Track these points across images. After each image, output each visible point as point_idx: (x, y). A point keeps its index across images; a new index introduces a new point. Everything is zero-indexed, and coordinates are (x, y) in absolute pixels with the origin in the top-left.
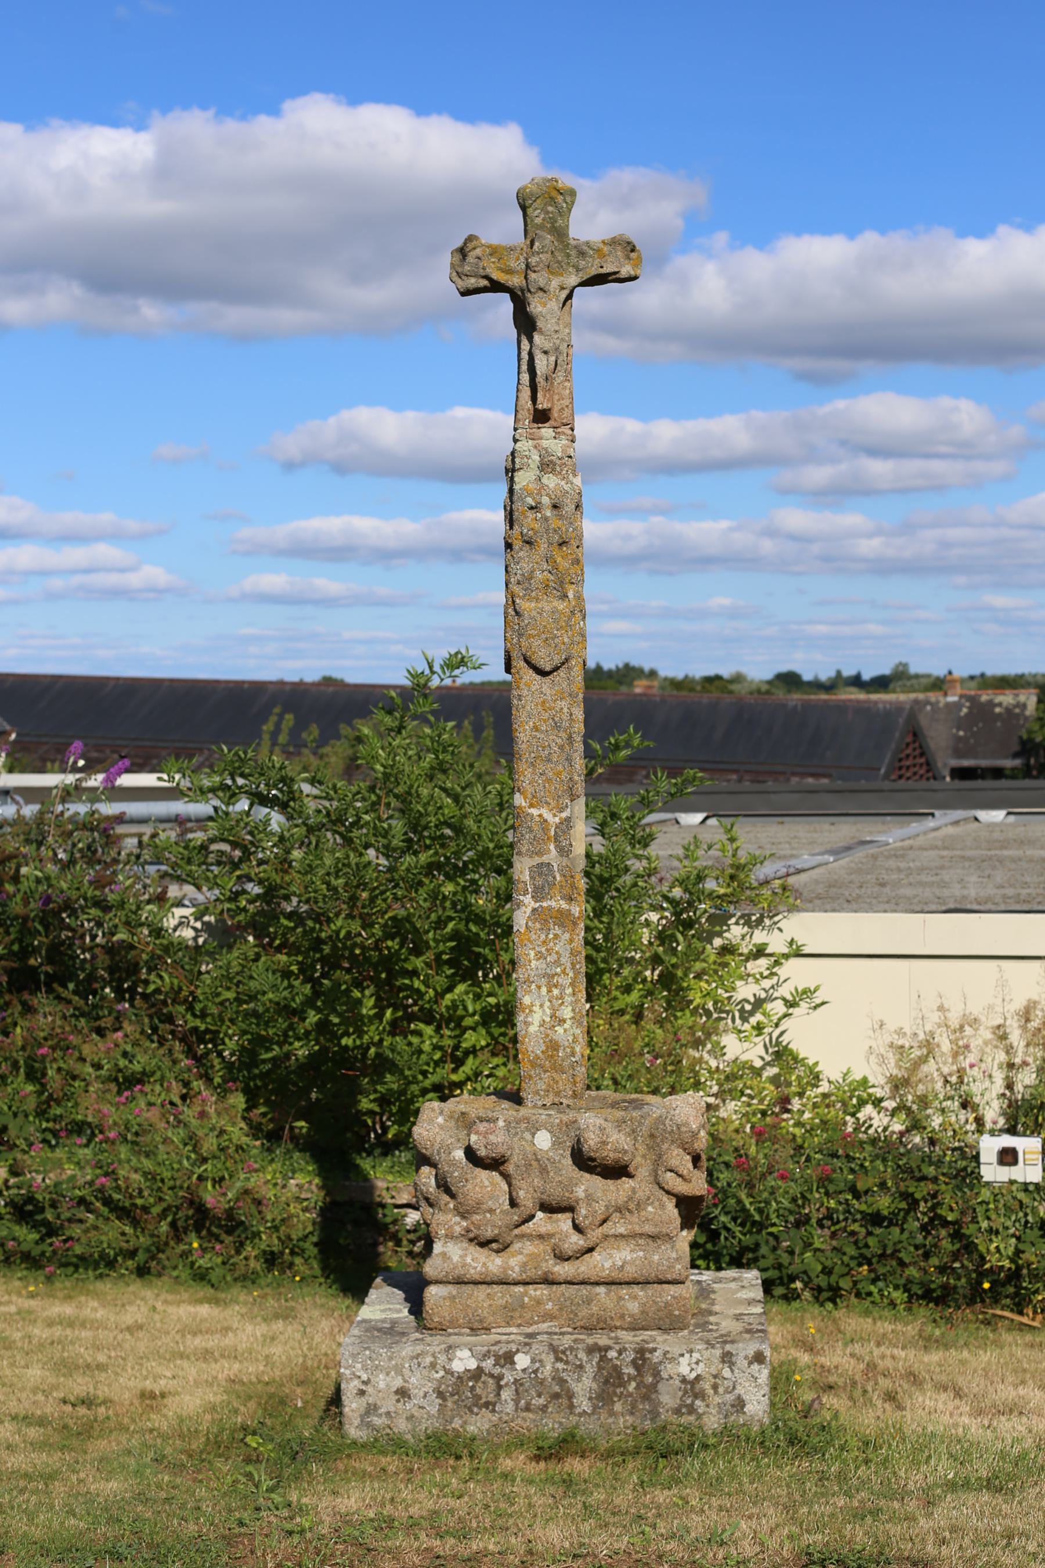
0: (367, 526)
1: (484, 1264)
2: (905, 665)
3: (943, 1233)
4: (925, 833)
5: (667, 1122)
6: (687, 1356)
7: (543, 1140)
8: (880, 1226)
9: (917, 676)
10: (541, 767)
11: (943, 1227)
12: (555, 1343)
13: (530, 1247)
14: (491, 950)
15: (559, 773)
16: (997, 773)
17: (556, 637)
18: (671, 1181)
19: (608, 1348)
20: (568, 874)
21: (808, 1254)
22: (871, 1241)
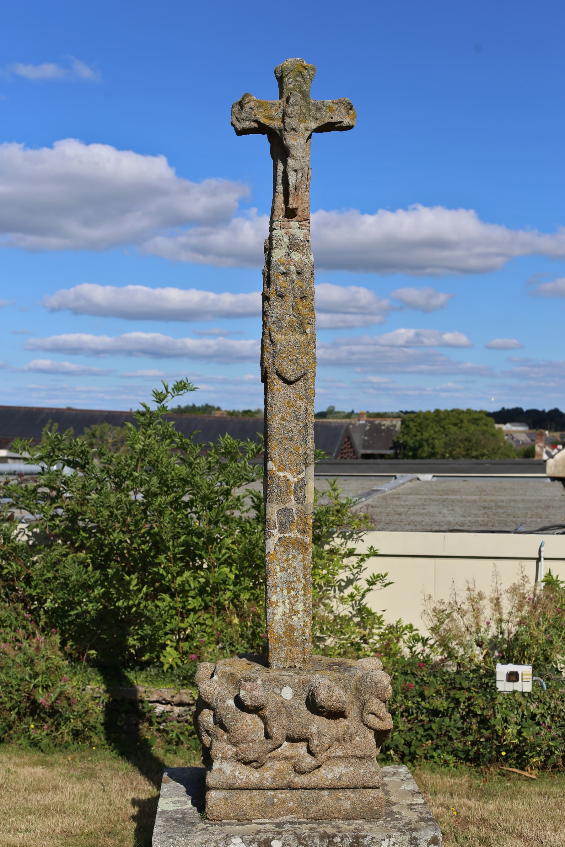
0: (88, 339)
1: (248, 776)
2: (333, 407)
3: (474, 721)
4: (399, 486)
5: (368, 680)
6: (387, 840)
7: (287, 693)
8: (437, 717)
9: (338, 412)
10: (285, 445)
11: (474, 717)
12: (298, 832)
13: (278, 765)
14: (206, 553)
15: (298, 449)
16: (382, 456)
17: (298, 358)
18: (372, 720)
19: (334, 836)
20: (302, 515)
21: (396, 733)
22: (434, 726)
